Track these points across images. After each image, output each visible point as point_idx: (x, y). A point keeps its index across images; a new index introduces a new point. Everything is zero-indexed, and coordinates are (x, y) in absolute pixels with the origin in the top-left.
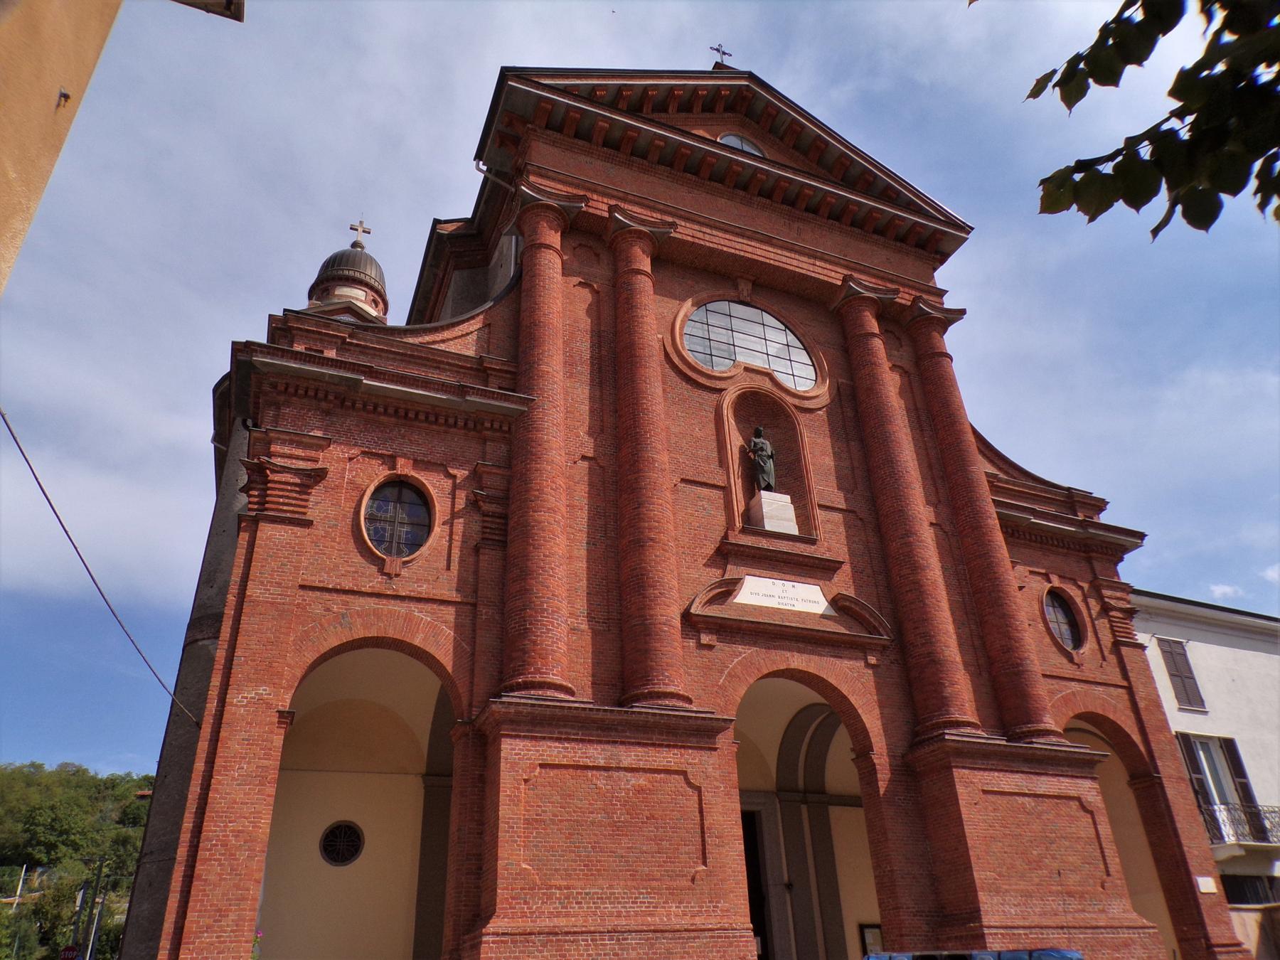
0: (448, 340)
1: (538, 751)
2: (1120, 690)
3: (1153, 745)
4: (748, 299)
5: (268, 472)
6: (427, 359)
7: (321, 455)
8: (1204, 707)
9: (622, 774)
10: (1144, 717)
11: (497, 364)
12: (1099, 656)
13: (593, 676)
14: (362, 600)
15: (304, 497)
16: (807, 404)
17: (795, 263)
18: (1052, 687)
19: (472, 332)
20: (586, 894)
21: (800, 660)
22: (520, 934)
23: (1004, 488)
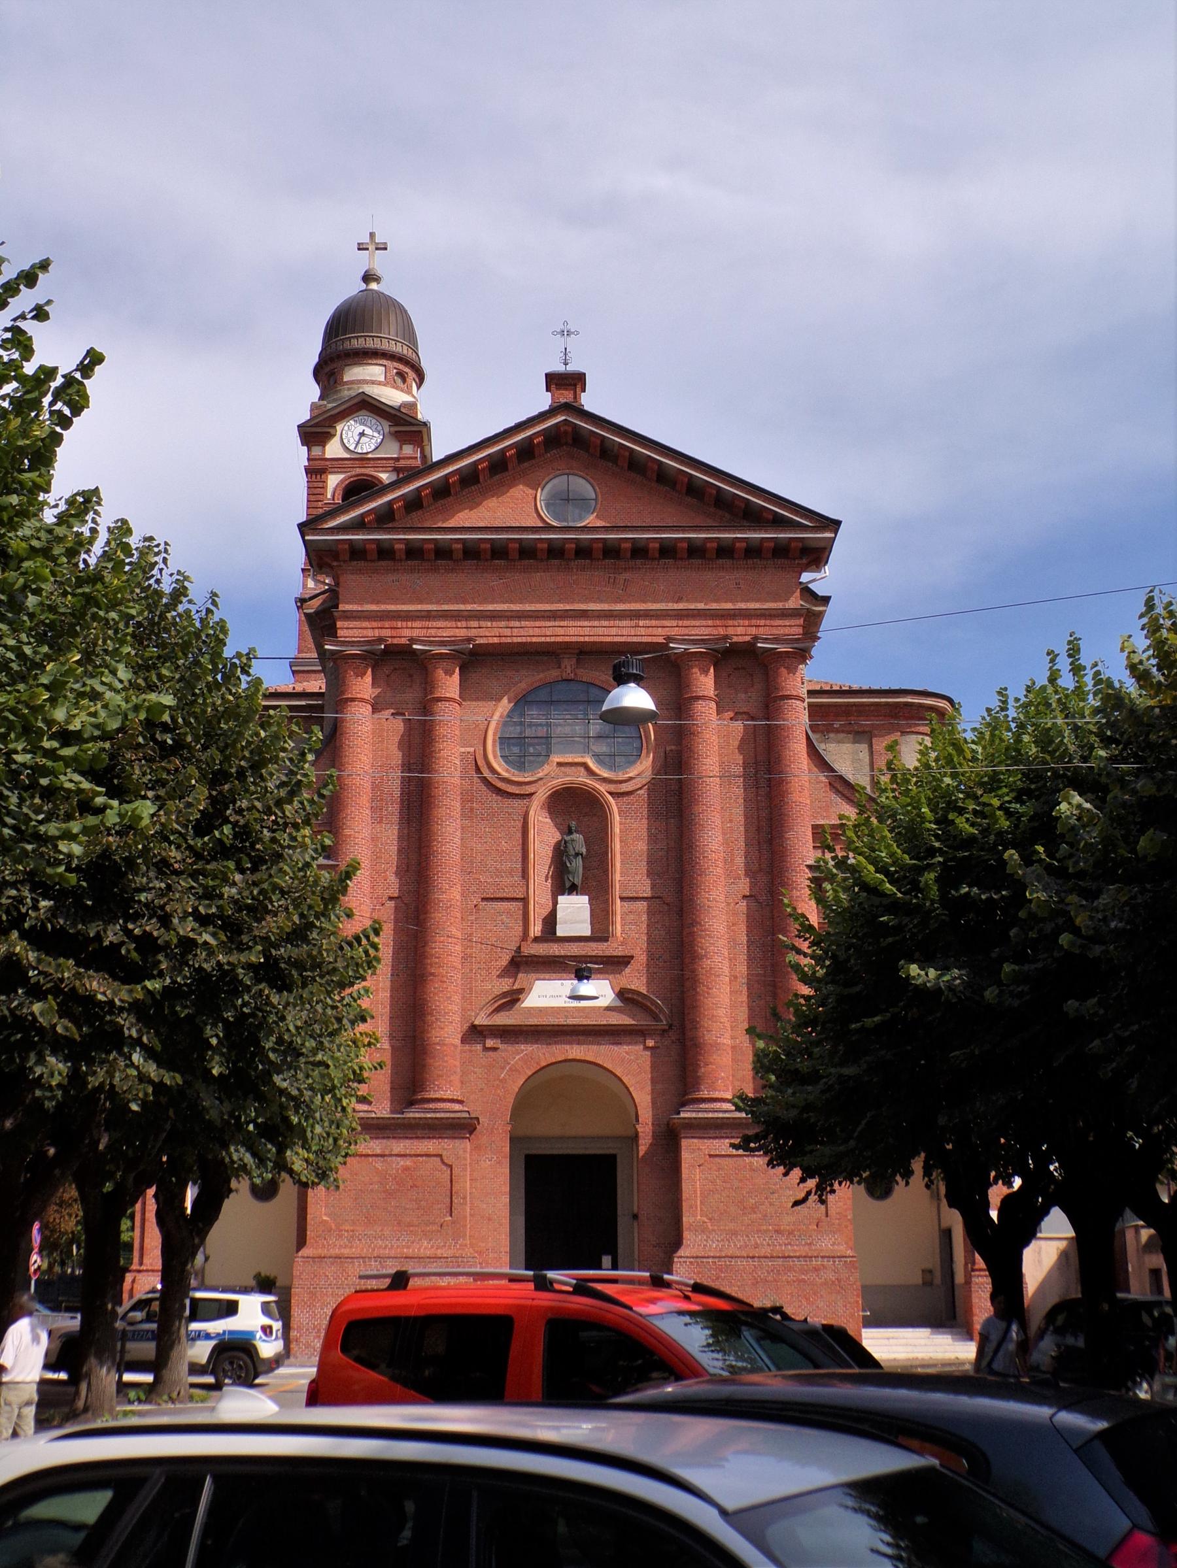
9: (394, 1158)
16: (625, 788)
17: (613, 631)
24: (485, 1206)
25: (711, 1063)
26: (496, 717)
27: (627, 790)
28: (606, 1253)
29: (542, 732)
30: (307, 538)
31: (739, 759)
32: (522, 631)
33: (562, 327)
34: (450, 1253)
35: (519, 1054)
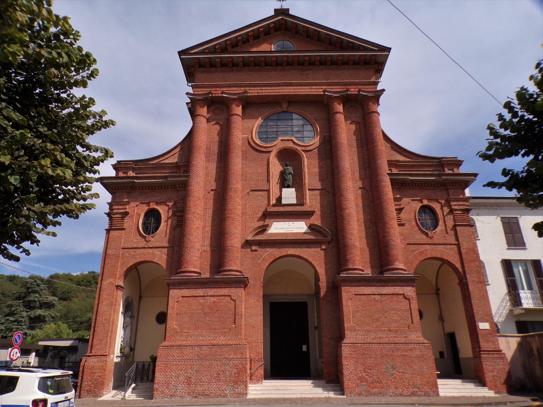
0: (168, 158)
1: (181, 292)
2: (453, 246)
4: (286, 110)
5: (112, 215)
6: (160, 167)
7: (128, 206)
8: (525, 247)
9: (208, 297)
10: (464, 256)
11: (182, 163)
12: (445, 232)
14: (140, 250)
15: (123, 221)
16: (308, 148)
17: (302, 90)
18: (414, 248)
19: (176, 153)
22: (170, 346)
23: (403, 165)
24: (251, 321)
25: (353, 254)
27: (309, 149)
28: (304, 344)
30: (181, 57)
31: (354, 138)
32: (266, 91)
34: (234, 342)
35: (266, 252)
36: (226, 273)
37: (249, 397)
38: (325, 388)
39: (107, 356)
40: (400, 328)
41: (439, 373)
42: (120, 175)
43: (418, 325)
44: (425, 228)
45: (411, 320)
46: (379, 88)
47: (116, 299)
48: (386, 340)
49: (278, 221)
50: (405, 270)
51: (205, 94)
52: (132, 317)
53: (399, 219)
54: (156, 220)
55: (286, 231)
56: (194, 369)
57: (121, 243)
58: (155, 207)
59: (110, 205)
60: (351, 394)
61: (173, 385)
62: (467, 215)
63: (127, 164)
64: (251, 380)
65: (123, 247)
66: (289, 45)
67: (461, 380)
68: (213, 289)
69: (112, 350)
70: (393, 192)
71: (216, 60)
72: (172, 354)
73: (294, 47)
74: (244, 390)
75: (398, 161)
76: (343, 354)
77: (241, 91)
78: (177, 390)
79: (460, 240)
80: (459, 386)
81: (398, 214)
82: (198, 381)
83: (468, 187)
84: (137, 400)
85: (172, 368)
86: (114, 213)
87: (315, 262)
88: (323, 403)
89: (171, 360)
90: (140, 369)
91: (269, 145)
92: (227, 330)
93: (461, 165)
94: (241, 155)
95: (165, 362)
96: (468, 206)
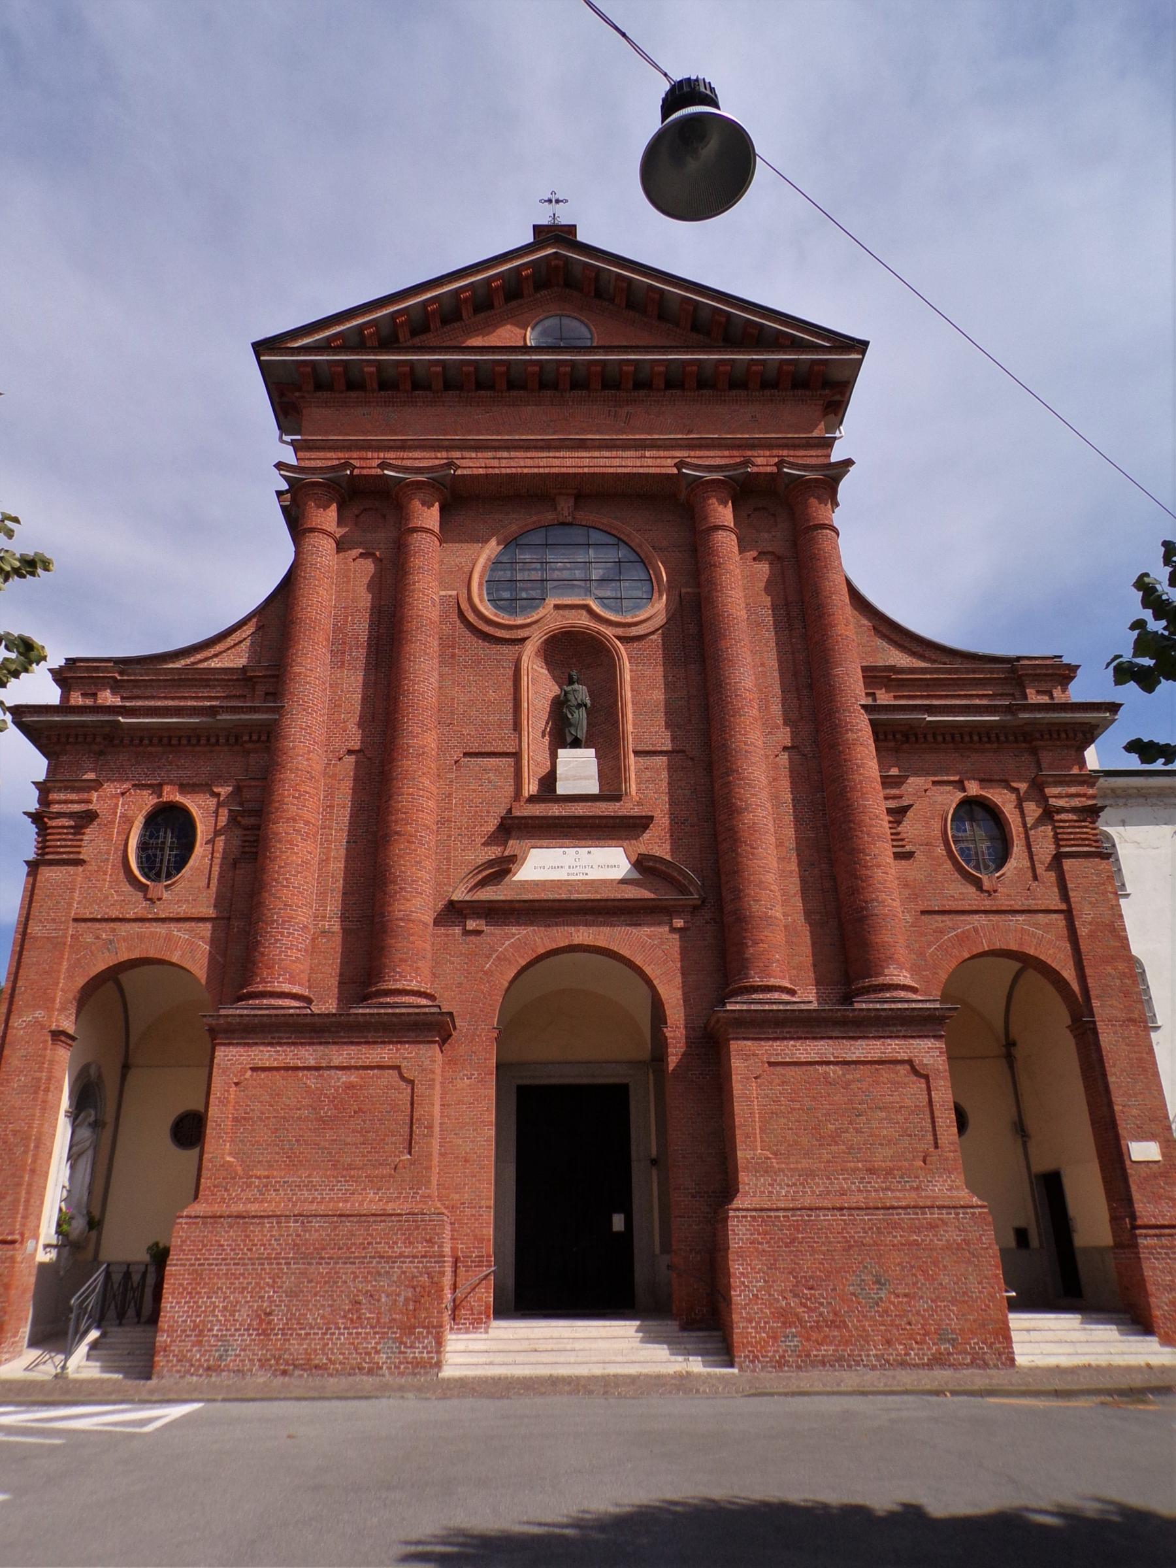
1: (250, 1056)
2: (1055, 916)
3: (1089, 980)
4: (570, 519)
5: (46, 820)
6: (196, 680)
7: (95, 795)
9: (333, 1072)
12: (1030, 874)
13: (341, 975)
14: (128, 926)
15: (79, 837)
17: (617, 462)
18: (941, 925)
19: (245, 639)
20: (284, 1182)
21: (586, 934)
22: (210, 1217)
24: (460, 1142)
26: (482, 561)
27: (638, 634)
29: (537, 575)
30: (262, 358)
31: (767, 601)
33: (550, 196)
34: (406, 1207)
36: (388, 1000)
37: (447, 1372)
38: (679, 1343)
39: (17, 1245)
40: (899, 1164)
41: (1014, 1294)
42: (73, 702)
43: (953, 1152)
44: (973, 864)
45: (932, 1138)
46: (837, 455)
47: (50, 1071)
48: (857, 1199)
49: (545, 845)
50: (913, 990)
51: (332, 468)
52: (97, 1125)
53: (897, 838)
54: (179, 838)
55: (568, 874)
56: (282, 1287)
57: (70, 905)
58: (179, 798)
59: (43, 788)
60: (752, 1362)
61: (217, 1336)
62: (1091, 826)
63: (97, 669)
64: (454, 1319)
65: (78, 916)
66: (578, 329)
67: (1079, 1316)
68: (345, 1047)
69: (31, 1225)
70: (879, 761)
71: (366, 369)
72: (216, 1241)
73: (591, 334)
74: (431, 1352)
75: (892, 669)
76: (731, 1242)
77: (437, 462)
78: (227, 1351)
79: (1072, 900)
80: (1072, 1332)
81: (895, 825)
82: (293, 1324)
83: (1093, 741)
84: (102, 1381)
85: (214, 1284)
86: (52, 813)
87: (652, 966)
88: (670, 1392)
89: (213, 1259)
90: (116, 1286)
91: (520, 622)
92: (387, 1171)
93: (1073, 678)
94: (436, 649)
95: (194, 1265)
96: (1093, 797)
